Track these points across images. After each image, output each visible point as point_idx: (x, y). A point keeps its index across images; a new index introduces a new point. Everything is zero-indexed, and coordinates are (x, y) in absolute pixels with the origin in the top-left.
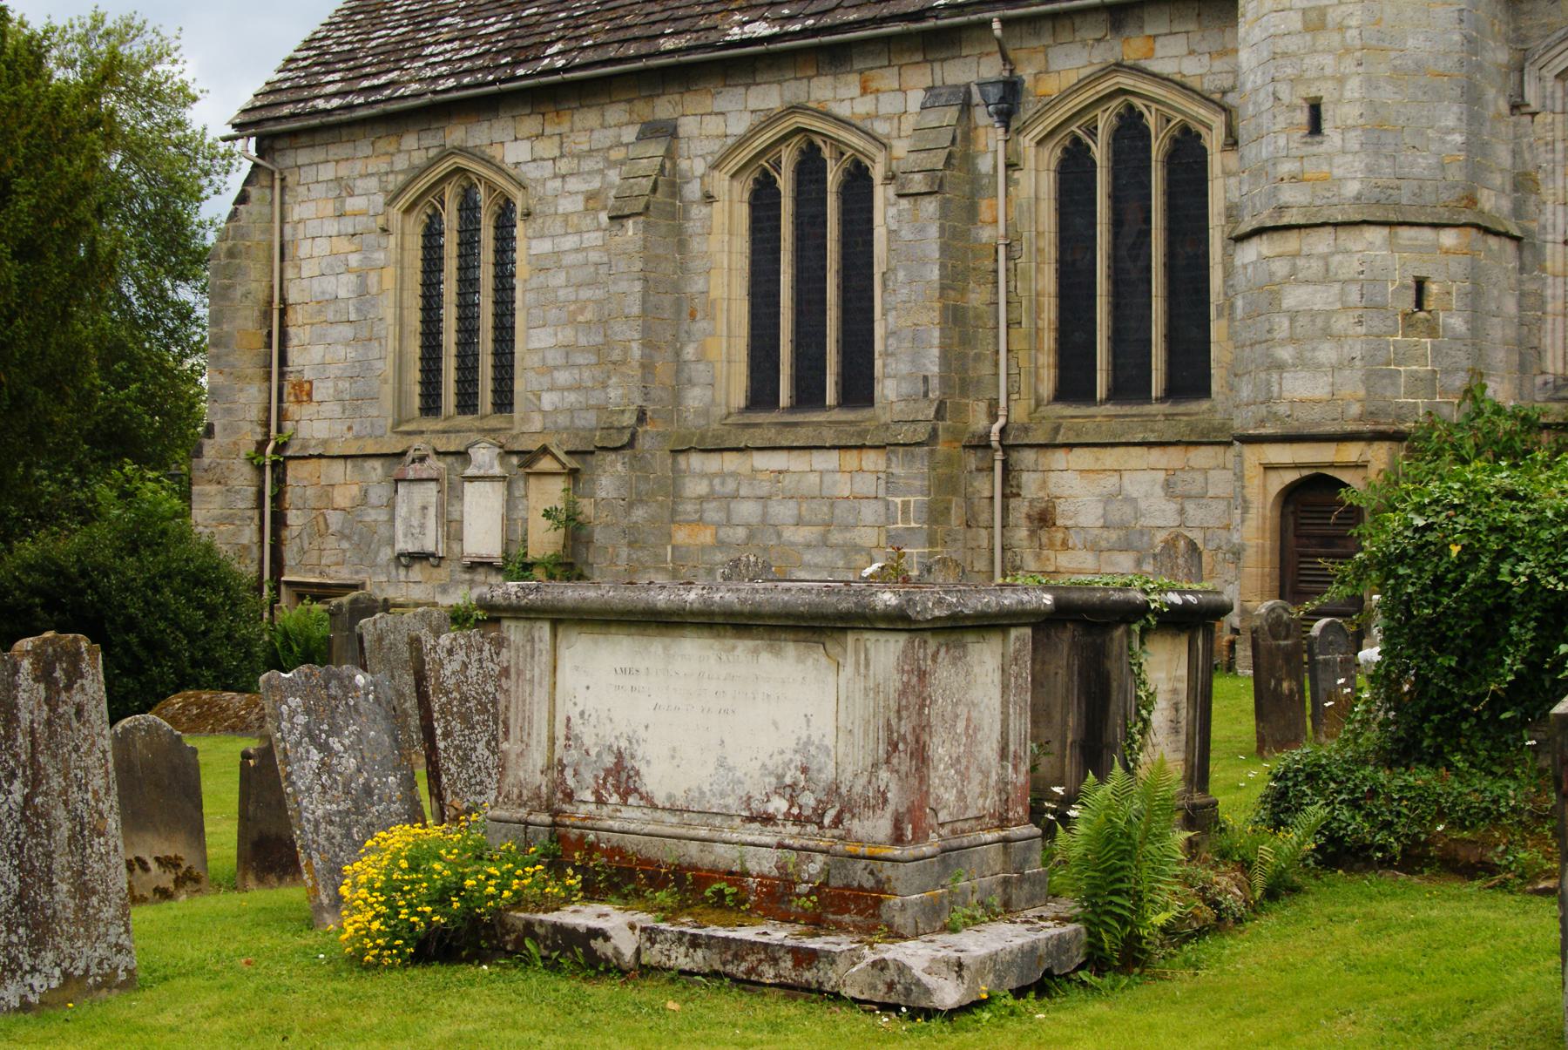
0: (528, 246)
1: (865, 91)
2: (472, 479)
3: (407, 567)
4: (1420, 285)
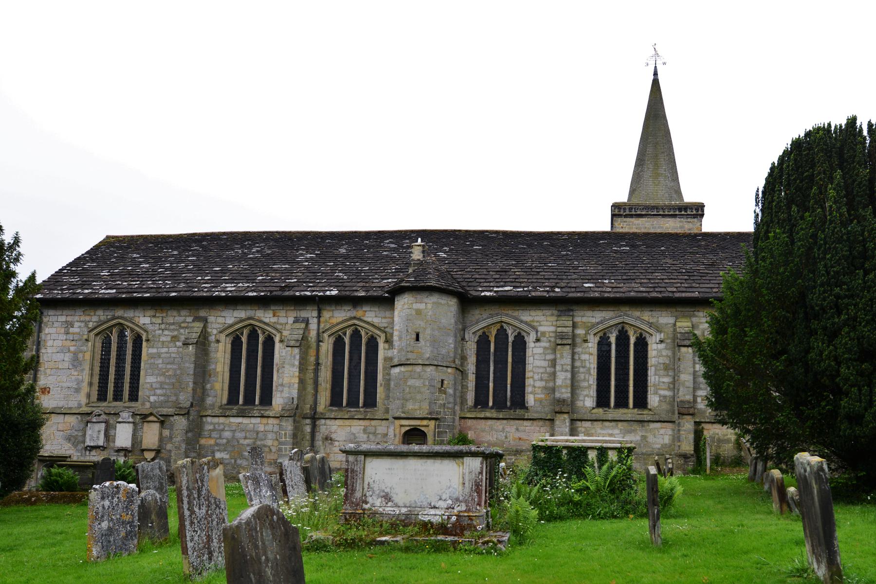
0: (146, 351)
1: (274, 316)
2: (120, 422)
3: (90, 451)
4: (442, 381)
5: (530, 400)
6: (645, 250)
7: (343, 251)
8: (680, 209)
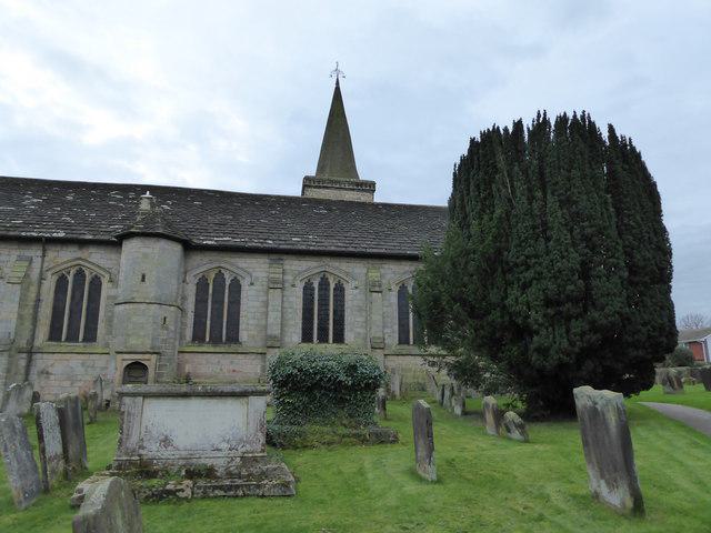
5: (244, 336)
6: (330, 210)
7: (69, 198)
8: (357, 184)
